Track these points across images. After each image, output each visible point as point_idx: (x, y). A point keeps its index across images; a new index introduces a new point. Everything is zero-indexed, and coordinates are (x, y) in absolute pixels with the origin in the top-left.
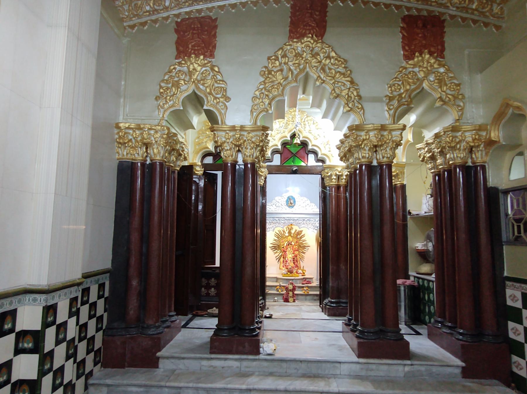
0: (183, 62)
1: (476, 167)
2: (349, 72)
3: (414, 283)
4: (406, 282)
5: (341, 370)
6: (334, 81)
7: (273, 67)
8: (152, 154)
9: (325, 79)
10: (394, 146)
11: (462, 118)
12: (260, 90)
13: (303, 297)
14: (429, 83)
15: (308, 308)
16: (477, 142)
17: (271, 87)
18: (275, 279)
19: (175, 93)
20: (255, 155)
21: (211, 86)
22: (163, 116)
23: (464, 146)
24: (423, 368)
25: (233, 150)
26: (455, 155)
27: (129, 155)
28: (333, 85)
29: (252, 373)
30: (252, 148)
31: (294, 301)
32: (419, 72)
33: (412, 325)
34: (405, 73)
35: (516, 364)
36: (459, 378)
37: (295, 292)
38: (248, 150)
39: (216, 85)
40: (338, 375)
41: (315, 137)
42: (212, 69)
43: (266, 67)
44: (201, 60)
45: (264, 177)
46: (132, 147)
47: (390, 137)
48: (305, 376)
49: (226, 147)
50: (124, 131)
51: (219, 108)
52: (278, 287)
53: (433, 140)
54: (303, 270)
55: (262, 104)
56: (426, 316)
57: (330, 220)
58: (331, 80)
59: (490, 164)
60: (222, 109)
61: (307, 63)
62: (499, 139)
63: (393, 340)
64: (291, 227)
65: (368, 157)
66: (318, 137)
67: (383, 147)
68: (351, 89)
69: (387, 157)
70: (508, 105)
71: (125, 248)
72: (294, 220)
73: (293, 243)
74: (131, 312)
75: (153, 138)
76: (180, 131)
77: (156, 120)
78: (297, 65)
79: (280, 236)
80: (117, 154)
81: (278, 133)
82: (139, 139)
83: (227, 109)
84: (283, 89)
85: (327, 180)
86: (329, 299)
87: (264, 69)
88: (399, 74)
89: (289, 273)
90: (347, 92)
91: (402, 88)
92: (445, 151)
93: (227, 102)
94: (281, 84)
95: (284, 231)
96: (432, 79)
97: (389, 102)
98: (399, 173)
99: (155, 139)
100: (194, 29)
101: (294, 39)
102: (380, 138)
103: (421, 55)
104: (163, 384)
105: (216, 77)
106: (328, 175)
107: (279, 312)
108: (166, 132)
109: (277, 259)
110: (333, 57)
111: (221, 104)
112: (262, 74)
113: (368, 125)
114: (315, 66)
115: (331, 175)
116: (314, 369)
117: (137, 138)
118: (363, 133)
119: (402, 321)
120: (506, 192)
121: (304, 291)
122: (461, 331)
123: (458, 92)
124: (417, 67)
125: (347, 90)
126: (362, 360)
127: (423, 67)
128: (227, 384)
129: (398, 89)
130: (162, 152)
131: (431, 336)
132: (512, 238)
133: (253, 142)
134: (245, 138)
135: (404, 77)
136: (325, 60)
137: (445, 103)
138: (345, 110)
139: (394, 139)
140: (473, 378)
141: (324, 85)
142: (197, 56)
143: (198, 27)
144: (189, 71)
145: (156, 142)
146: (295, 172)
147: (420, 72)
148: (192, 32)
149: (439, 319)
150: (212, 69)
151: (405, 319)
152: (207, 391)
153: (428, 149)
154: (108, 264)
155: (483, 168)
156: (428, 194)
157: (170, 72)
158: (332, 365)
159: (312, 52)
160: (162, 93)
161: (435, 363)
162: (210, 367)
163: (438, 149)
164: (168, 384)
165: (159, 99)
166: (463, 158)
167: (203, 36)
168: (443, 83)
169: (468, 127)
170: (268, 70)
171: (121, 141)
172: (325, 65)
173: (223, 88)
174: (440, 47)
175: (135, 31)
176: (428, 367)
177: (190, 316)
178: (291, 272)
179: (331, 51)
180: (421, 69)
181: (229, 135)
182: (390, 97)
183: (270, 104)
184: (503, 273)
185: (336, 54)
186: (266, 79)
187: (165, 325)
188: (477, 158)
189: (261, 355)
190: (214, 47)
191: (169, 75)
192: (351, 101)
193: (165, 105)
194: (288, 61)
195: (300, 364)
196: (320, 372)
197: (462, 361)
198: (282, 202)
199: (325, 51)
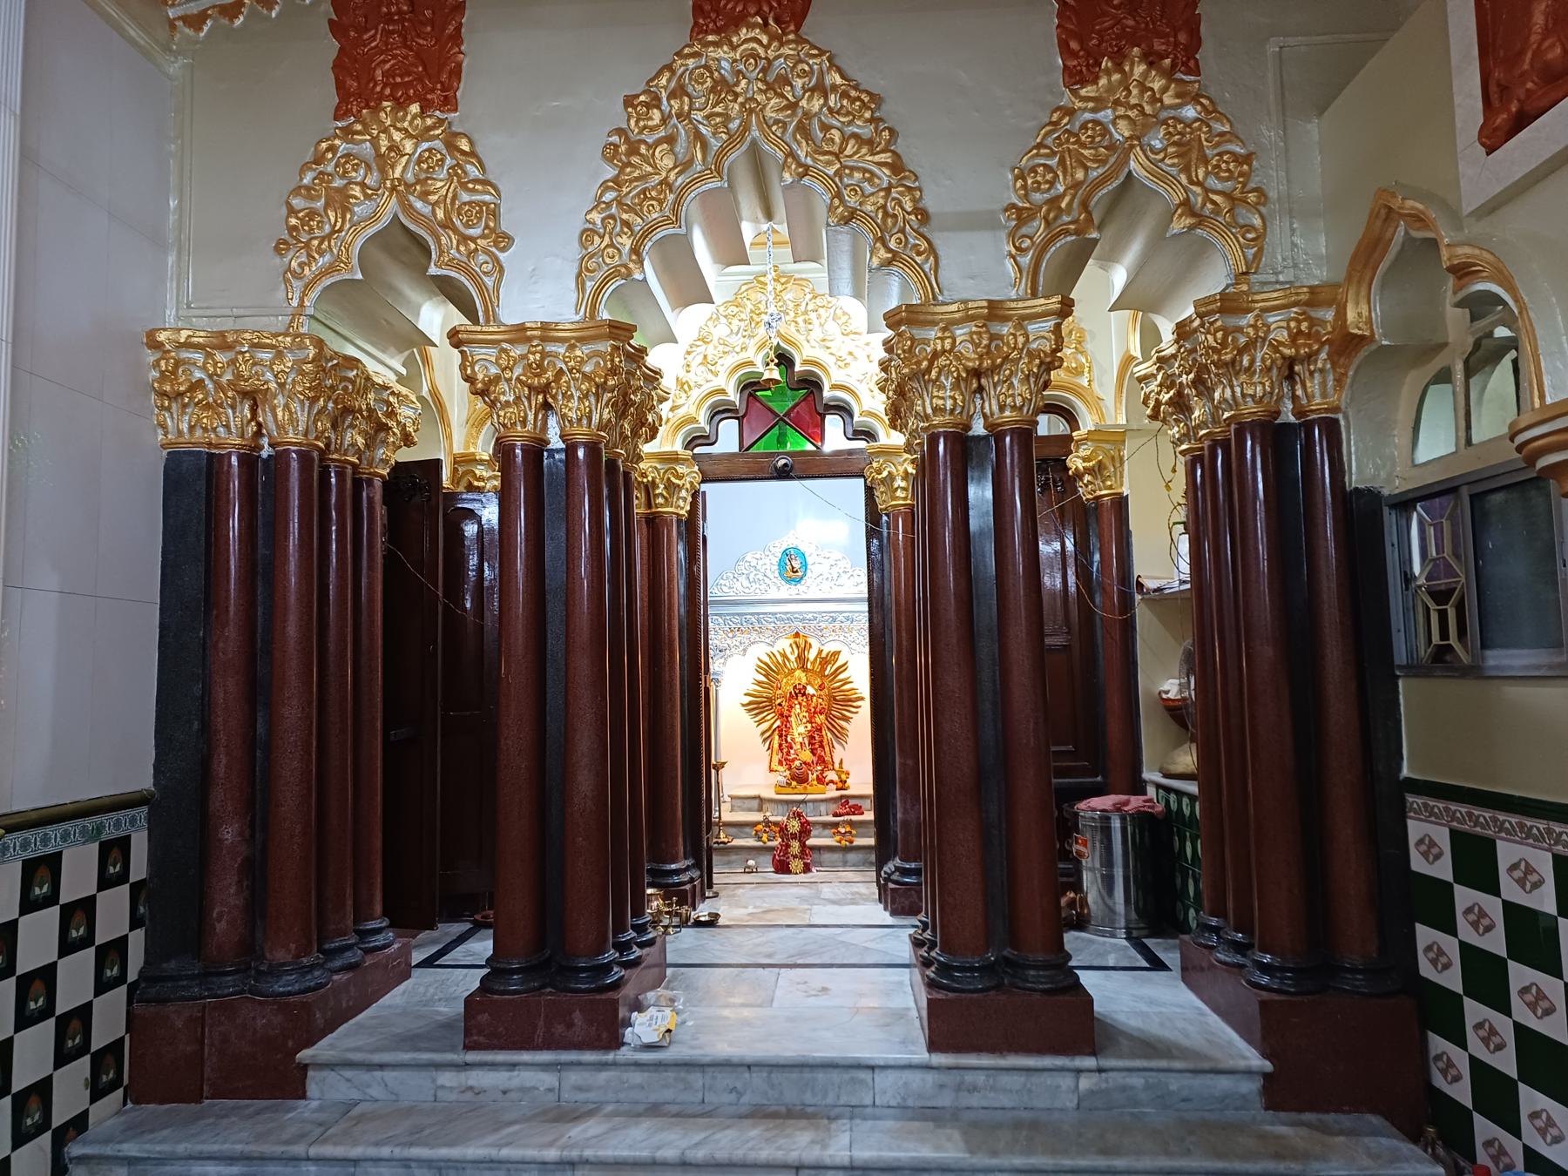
0: (359, 127)
1: (1308, 427)
2: (886, 134)
3: (1152, 807)
4: (1127, 803)
5: (876, 1091)
6: (838, 166)
7: (640, 132)
8: (272, 426)
9: (809, 161)
10: (1035, 370)
11: (1257, 267)
12: (604, 206)
13: (836, 856)
14: (1147, 157)
15: (838, 891)
16: (1305, 345)
17: (638, 195)
18: (755, 803)
19: (337, 228)
20: (595, 419)
21: (448, 201)
22: (301, 304)
23: (1263, 360)
24: (1137, 1081)
25: (526, 404)
26: (1238, 390)
27: (198, 433)
28: (837, 179)
29: (594, 1106)
30: (586, 396)
31: (807, 869)
32: (1114, 123)
33: (1147, 937)
34: (1068, 127)
35: (1441, 1064)
36: (1257, 1112)
37: (811, 842)
38: (574, 403)
39: (465, 197)
40: (865, 1106)
41: (839, 359)
42: (451, 146)
43: (620, 131)
44: (414, 117)
45: (687, 490)
46: (208, 406)
47: (1021, 340)
48: (759, 1114)
49: (504, 393)
50: (173, 354)
51: (477, 269)
52: (760, 827)
53: (1176, 346)
54: (839, 773)
55: (610, 250)
56: (1188, 910)
57: (372, 622)
58: (829, 163)
59: (1351, 413)
60: (484, 273)
61: (751, 111)
62: (1372, 330)
63: (1044, 991)
64: (806, 642)
65: (952, 411)
66: (849, 360)
67: (999, 374)
68: (893, 190)
69: (1014, 408)
70: (1389, 215)
71: (196, 725)
72: (804, 619)
73: (810, 690)
74: (221, 927)
75: (269, 376)
76: (383, 352)
77: (280, 318)
78: (718, 120)
79: (771, 671)
80: (160, 431)
81: (725, 353)
82: (228, 376)
83: (502, 271)
84: (678, 202)
85: (882, 493)
86: (898, 862)
87: (615, 139)
88: (1048, 134)
89: (794, 783)
90: (882, 201)
91: (1061, 177)
92: (1209, 377)
93: (503, 250)
94: (670, 186)
95: (784, 655)
96: (1158, 144)
97: (1017, 227)
98: (1104, 461)
99: (276, 376)
100: (389, 19)
101: (707, 33)
102: (988, 346)
103: (1119, 67)
104: (298, 1149)
105: (465, 172)
106: (880, 477)
107: (746, 907)
108: (312, 352)
109: (765, 740)
110: (834, 88)
111: (482, 258)
112: (610, 152)
113: (947, 304)
114: (777, 122)
115: (891, 477)
116: (790, 1091)
117: (217, 375)
118: (933, 333)
119: (1117, 926)
120: (1404, 504)
121: (838, 838)
122: (1267, 959)
123: (1244, 185)
124: (1106, 108)
125: (882, 194)
126: (940, 1059)
127: (1128, 103)
128: (500, 1146)
129: (1047, 182)
130: (302, 418)
131: (1190, 974)
132: (1426, 652)
133: (586, 377)
134: (561, 365)
135: (1068, 141)
136: (810, 100)
137: (1200, 220)
138: (875, 262)
139: (1034, 346)
140: (1300, 1110)
141: (806, 181)
142: (401, 105)
143: (400, 12)
144: (379, 156)
145: (282, 386)
146: (784, 474)
147: (1118, 121)
148: (383, 29)
149: (1214, 922)
150: (451, 146)
151: (1128, 921)
152: (440, 1169)
153: (1167, 377)
154: (143, 779)
155: (1331, 429)
156: (1175, 524)
157: (319, 159)
158: (846, 1076)
159: (765, 76)
160: (295, 228)
161: (1178, 1065)
162: (463, 1092)
163: (1188, 374)
164: (313, 1152)
165: (288, 250)
166: (1261, 398)
167: (421, 42)
168: (1194, 156)
169: (1275, 295)
170: (627, 140)
171: (168, 388)
172: (807, 115)
173: (486, 204)
174: (1182, 38)
175: (205, 36)
176: (1153, 1078)
177: (468, 926)
178: (801, 779)
179: (829, 69)
180: (1121, 111)
181: (509, 356)
182: (1020, 210)
183: (636, 250)
184: (1399, 769)
185: (843, 77)
186: (622, 171)
187: (338, 963)
188: (1309, 397)
189: (624, 1049)
190: (457, 73)
191: (315, 170)
192: (896, 231)
193: (307, 268)
194: (691, 109)
195: (747, 1075)
196: (808, 1098)
197: (1265, 1055)
198: (764, 567)
199: (807, 68)
